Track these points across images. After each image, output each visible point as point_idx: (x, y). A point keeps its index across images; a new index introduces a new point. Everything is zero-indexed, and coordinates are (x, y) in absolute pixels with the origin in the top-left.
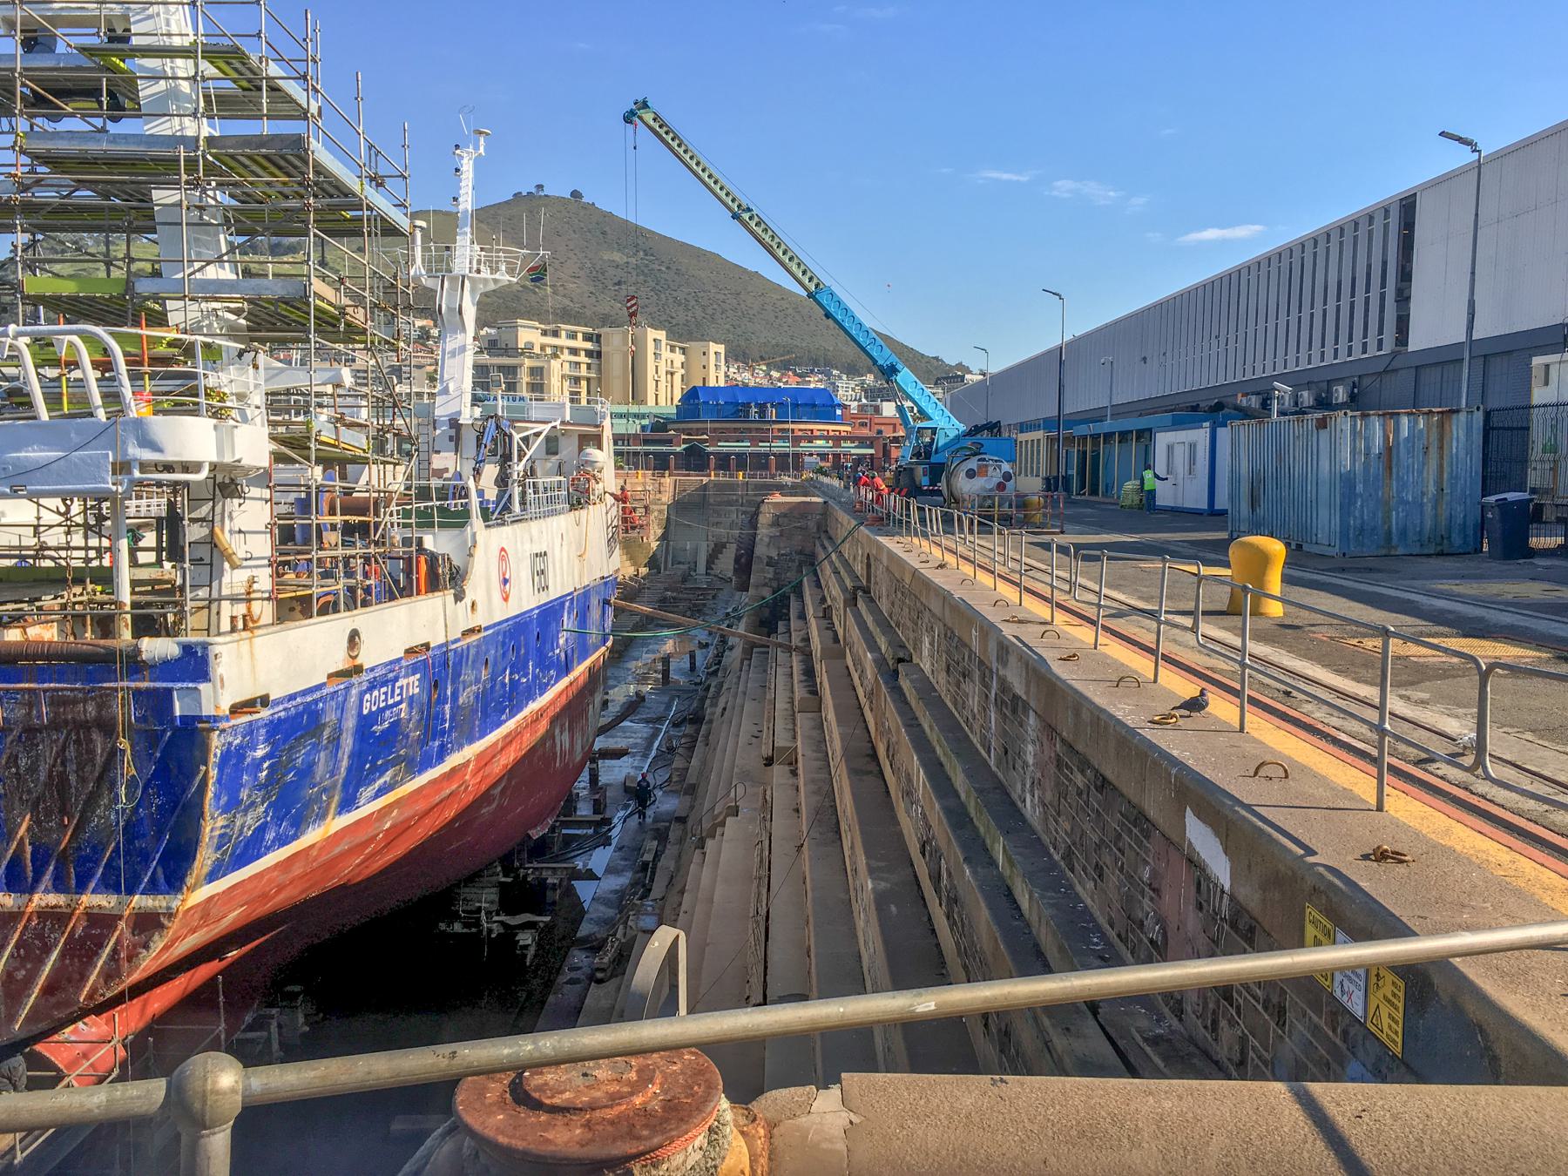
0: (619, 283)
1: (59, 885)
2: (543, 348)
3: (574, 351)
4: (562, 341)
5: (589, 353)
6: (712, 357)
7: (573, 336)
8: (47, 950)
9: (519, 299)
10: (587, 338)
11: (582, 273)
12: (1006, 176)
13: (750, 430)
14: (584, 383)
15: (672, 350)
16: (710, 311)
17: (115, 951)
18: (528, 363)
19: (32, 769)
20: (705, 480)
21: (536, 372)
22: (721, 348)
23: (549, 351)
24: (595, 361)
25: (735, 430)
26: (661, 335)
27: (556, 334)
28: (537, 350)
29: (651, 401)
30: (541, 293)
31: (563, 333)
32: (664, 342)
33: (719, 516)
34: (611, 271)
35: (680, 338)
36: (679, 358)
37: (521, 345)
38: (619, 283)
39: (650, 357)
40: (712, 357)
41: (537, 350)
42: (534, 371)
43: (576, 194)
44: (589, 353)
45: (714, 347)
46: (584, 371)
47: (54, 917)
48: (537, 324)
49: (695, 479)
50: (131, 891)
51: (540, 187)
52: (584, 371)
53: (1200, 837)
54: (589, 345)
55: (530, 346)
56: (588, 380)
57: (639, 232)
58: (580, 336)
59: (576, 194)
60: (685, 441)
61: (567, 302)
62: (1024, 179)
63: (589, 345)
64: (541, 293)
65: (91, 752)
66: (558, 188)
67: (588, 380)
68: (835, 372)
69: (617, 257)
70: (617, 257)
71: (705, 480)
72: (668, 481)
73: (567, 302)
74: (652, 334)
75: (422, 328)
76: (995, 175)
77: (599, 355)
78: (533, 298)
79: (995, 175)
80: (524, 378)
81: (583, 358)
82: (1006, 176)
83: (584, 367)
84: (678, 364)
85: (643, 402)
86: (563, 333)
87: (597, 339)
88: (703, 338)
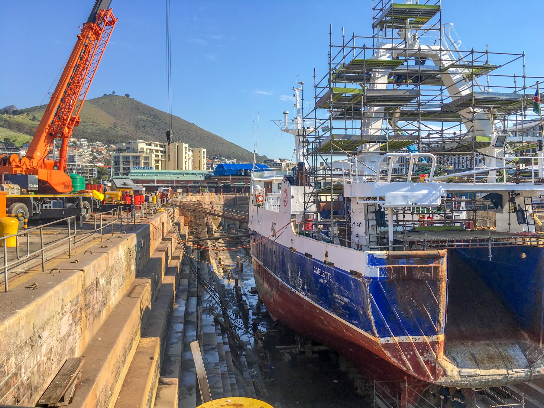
0: (144, 127)
2: (147, 149)
3: (157, 151)
5: (162, 152)
10: (161, 146)
11: (130, 123)
13: (243, 179)
14: (160, 162)
20: (234, 196)
21: (147, 158)
23: (148, 151)
24: (164, 154)
25: (238, 179)
27: (150, 145)
28: (145, 150)
29: (184, 169)
30: (117, 130)
33: (241, 208)
37: (139, 149)
38: (144, 127)
39: (184, 153)
41: (145, 150)
43: (127, 95)
44: (162, 152)
46: (160, 158)
49: (231, 196)
51: (114, 92)
53: (287, 292)
54: (162, 149)
55: (142, 149)
56: (162, 161)
57: (151, 109)
58: (159, 146)
59: (127, 95)
61: (126, 133)
62: (271, 94)
63: (162, 149)
64: (117, 130)
66: (121, 93)
67: (162, 161)
69: (143, 117)
70: (143, 117)
72: (222, 196)
73: (126, 133)
74: (185, 145)
75: (73, 142)
76: (261, 92)
77: (165, 152)
79: (261, 92)
80: (142, 160)
81: (160, 153)
83: (160, 156)
84: (190, 156)
85: (181, 169)
86: (159, 146)
87: (164, 147)
88: (201, 147)
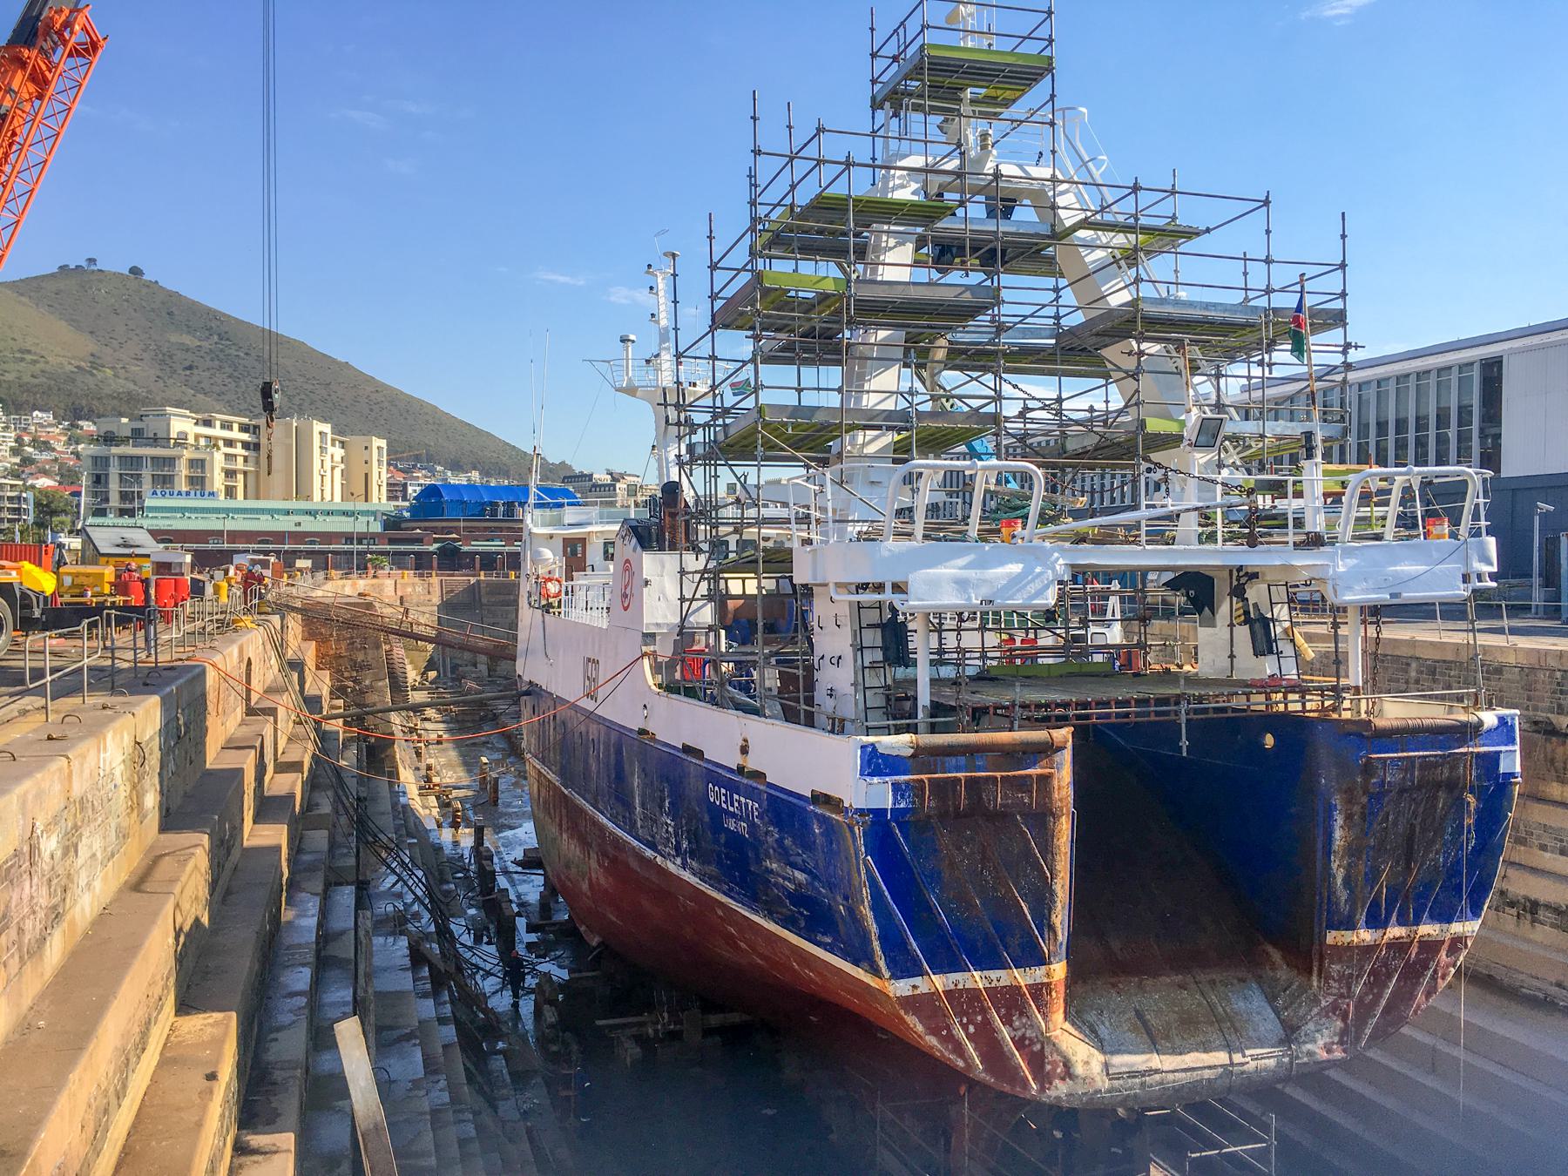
0: (190, 368)
1: (1402, 922)
2: (197, 437)
3: (230, 443)
4: (216, 431)
5: (246, 445)
6: (375, 451)
7: (227, 426)
8: (1390, 977)
9: (74, 381)
10: (244, 428)
11: (145, 355)
12: (562, 279)
13: (501, 529)
14: (240, 477)
15: (333, 445)
16: (297, 401)
17: (1435, 971)
18: (187, 454)
19: (1395, 824)
20: (473, 580)
22: (383, 443)
24: (253, 454)
25: (486, 529)
26: (327, 428)
28: (191, 440)
29: (317, 497)
31: (218, 424)
32: (329, 436)
34: (179, 355)
35: (341, 433)
36: (338, 452)
37: (173, 435)
38: (190, 368)
39: (316, 451)
40: (375, 451)
41: (191, 440)
42: (193, 463)
44: (246, 445)
45: (379, 443)
46: (240, 464)
47: (1398, 947)
48: (187, 412)
50: (1450, 922)
51: (92, 261)
52: (240, 464)
54: (245, 437)
55: (183, 436)
56: (245, 473)
58: (236, 426)
59: (135, 271)
60: (436, 541)
61: (132, 386)
64: (100, 376)
65: (1435, 807)
66: (115, 262)
67: (245, 473)
68: (439, 468)
69: (187, 340)
70: (187, 340)
71: (473, 580)
72: (435, 580)
73: (132, 386)
74: (319, 427)
77: (257, 447)
78: (91, 381)
80: (183, 470)
82: (562, 279)
83: (240, 460)
84: (338, 458)
85: (309, 498)
88: (369, 433)
